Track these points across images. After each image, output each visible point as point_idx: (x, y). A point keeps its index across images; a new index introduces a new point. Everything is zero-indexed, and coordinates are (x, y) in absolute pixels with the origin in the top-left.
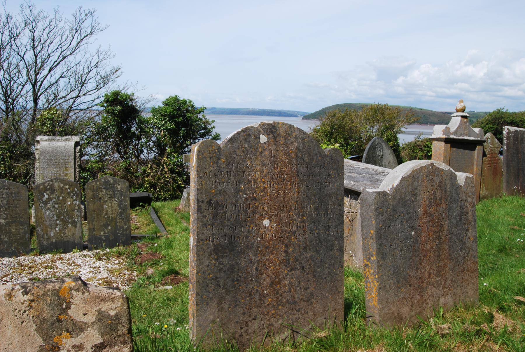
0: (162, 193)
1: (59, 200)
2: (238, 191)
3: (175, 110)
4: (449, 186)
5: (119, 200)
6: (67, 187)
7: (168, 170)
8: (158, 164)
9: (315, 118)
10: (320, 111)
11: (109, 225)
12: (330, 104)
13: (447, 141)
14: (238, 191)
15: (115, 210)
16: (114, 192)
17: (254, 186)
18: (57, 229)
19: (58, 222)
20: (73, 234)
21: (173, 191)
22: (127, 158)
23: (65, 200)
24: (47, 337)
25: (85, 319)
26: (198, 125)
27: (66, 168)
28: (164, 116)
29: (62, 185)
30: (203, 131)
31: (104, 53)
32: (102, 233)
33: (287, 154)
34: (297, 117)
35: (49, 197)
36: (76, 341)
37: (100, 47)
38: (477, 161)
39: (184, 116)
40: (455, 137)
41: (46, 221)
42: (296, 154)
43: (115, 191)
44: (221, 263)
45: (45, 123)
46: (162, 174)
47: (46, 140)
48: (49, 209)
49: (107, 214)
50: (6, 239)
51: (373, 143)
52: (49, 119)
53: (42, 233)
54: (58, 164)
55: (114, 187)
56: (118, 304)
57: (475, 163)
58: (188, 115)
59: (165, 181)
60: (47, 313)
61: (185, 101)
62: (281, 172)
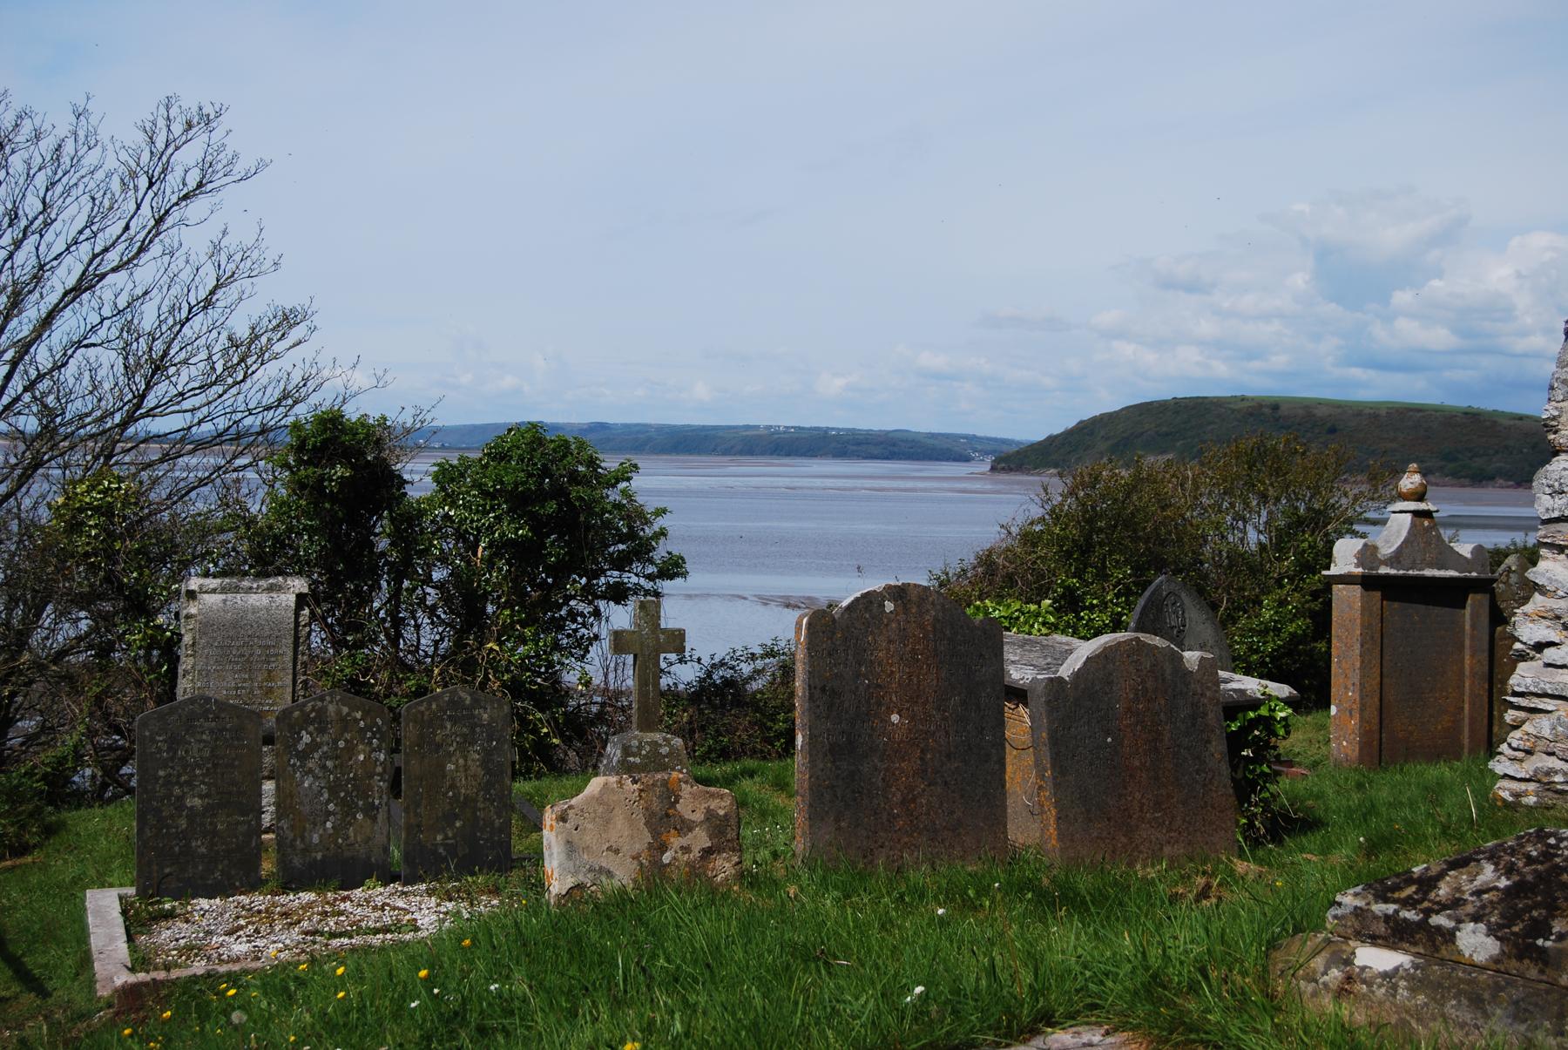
1: (337, 748)
2: (858, 675)
3: (530, 475)
4: (1168, 672)
5: (484, 749)
6: (359, 715)
7: (504, 685)
9: (1048, 465)
10: (1069, 433)
11: (456, 817)
12: (1108, 401)
13: (1369, 582)
14: (858, 675)
15: (474, 776)
16: (472, 728)
17: (878, 669)
18: (329, 825)
19: (331, 807)
20: (368, 840)
22: (359, 645)
23: (351, 750)
24: (655, 834)
25: (694, 817)
26: (607, 525)
27: (270, 672)
28: (493, 496)
29: (345, 710)
30: (621, 547)
31: (238, 257)
32: (439, 837)
33: (922, 627)
34: (966, 459)
35: (313, 740)
36: (683, 841)
37: (225, 233)
38: (1472, 637)
39: (559, 493)
40: (1393, 572)
41: (301, 803)
42: (934, 627)
43: (476, 725)
44: (838, 768)
45: (83, 524)
47: (214, 591)
48: (311, 771)
49: (452, 787)
50: (203, 850)
51: (1153, 593)
52: (96, 510)
53: (291, 835)
54: (248, 661)
55: (473, 716)
56: (727, 802)
57: (1467, 643)
58: (576, 491)
60: (656, 806)
62: (914, 652)
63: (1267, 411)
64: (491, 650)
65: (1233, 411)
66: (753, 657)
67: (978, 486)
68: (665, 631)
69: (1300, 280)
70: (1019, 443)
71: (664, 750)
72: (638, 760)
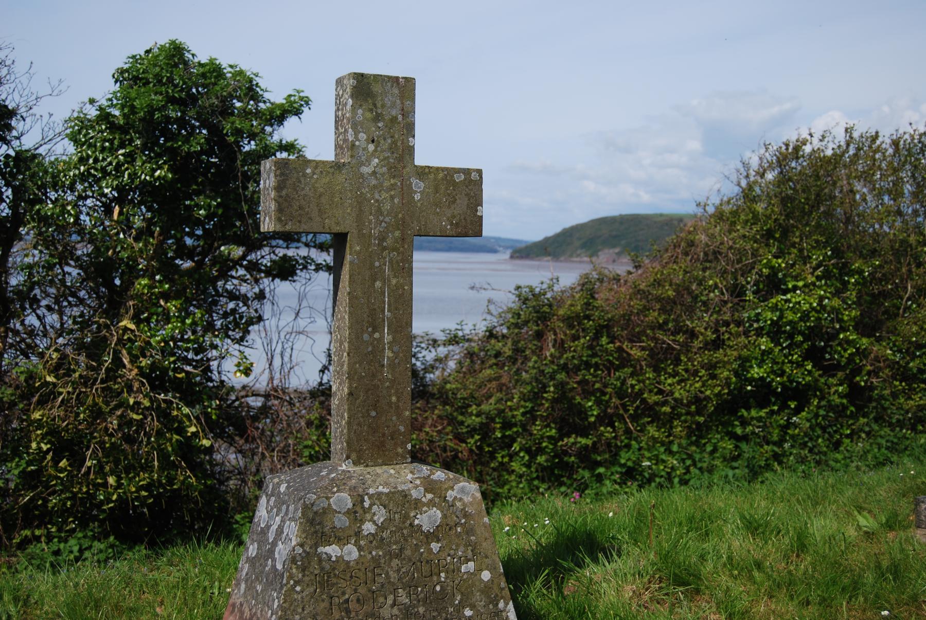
0: (111, 480)
7: (141, 372)
8: (95, 350)
10: (557, 236)
21: (162, 468)
28: (123, 130)
34: (495, 251)
46: (107, 391)
59: (125, 422)
61: (214, 71)
63: (676, 223)
64: (126, 329)
65: (655, 222)
66: (435, 343)
67: (503, 267)
68: (424, 172)
69: (695, 145)
70: (526, 242)
71: (429, 519)
72: (351, 552)
